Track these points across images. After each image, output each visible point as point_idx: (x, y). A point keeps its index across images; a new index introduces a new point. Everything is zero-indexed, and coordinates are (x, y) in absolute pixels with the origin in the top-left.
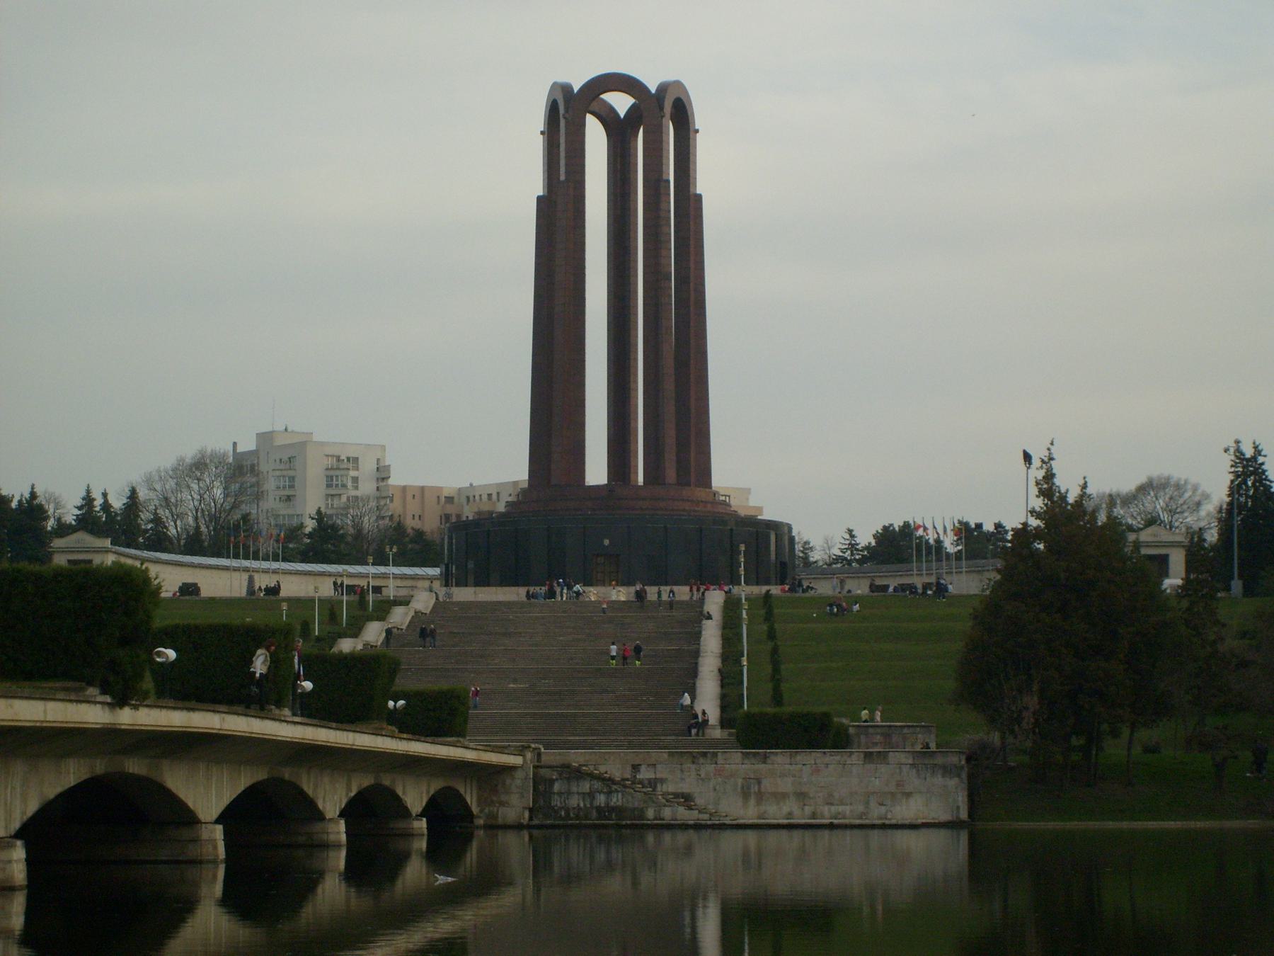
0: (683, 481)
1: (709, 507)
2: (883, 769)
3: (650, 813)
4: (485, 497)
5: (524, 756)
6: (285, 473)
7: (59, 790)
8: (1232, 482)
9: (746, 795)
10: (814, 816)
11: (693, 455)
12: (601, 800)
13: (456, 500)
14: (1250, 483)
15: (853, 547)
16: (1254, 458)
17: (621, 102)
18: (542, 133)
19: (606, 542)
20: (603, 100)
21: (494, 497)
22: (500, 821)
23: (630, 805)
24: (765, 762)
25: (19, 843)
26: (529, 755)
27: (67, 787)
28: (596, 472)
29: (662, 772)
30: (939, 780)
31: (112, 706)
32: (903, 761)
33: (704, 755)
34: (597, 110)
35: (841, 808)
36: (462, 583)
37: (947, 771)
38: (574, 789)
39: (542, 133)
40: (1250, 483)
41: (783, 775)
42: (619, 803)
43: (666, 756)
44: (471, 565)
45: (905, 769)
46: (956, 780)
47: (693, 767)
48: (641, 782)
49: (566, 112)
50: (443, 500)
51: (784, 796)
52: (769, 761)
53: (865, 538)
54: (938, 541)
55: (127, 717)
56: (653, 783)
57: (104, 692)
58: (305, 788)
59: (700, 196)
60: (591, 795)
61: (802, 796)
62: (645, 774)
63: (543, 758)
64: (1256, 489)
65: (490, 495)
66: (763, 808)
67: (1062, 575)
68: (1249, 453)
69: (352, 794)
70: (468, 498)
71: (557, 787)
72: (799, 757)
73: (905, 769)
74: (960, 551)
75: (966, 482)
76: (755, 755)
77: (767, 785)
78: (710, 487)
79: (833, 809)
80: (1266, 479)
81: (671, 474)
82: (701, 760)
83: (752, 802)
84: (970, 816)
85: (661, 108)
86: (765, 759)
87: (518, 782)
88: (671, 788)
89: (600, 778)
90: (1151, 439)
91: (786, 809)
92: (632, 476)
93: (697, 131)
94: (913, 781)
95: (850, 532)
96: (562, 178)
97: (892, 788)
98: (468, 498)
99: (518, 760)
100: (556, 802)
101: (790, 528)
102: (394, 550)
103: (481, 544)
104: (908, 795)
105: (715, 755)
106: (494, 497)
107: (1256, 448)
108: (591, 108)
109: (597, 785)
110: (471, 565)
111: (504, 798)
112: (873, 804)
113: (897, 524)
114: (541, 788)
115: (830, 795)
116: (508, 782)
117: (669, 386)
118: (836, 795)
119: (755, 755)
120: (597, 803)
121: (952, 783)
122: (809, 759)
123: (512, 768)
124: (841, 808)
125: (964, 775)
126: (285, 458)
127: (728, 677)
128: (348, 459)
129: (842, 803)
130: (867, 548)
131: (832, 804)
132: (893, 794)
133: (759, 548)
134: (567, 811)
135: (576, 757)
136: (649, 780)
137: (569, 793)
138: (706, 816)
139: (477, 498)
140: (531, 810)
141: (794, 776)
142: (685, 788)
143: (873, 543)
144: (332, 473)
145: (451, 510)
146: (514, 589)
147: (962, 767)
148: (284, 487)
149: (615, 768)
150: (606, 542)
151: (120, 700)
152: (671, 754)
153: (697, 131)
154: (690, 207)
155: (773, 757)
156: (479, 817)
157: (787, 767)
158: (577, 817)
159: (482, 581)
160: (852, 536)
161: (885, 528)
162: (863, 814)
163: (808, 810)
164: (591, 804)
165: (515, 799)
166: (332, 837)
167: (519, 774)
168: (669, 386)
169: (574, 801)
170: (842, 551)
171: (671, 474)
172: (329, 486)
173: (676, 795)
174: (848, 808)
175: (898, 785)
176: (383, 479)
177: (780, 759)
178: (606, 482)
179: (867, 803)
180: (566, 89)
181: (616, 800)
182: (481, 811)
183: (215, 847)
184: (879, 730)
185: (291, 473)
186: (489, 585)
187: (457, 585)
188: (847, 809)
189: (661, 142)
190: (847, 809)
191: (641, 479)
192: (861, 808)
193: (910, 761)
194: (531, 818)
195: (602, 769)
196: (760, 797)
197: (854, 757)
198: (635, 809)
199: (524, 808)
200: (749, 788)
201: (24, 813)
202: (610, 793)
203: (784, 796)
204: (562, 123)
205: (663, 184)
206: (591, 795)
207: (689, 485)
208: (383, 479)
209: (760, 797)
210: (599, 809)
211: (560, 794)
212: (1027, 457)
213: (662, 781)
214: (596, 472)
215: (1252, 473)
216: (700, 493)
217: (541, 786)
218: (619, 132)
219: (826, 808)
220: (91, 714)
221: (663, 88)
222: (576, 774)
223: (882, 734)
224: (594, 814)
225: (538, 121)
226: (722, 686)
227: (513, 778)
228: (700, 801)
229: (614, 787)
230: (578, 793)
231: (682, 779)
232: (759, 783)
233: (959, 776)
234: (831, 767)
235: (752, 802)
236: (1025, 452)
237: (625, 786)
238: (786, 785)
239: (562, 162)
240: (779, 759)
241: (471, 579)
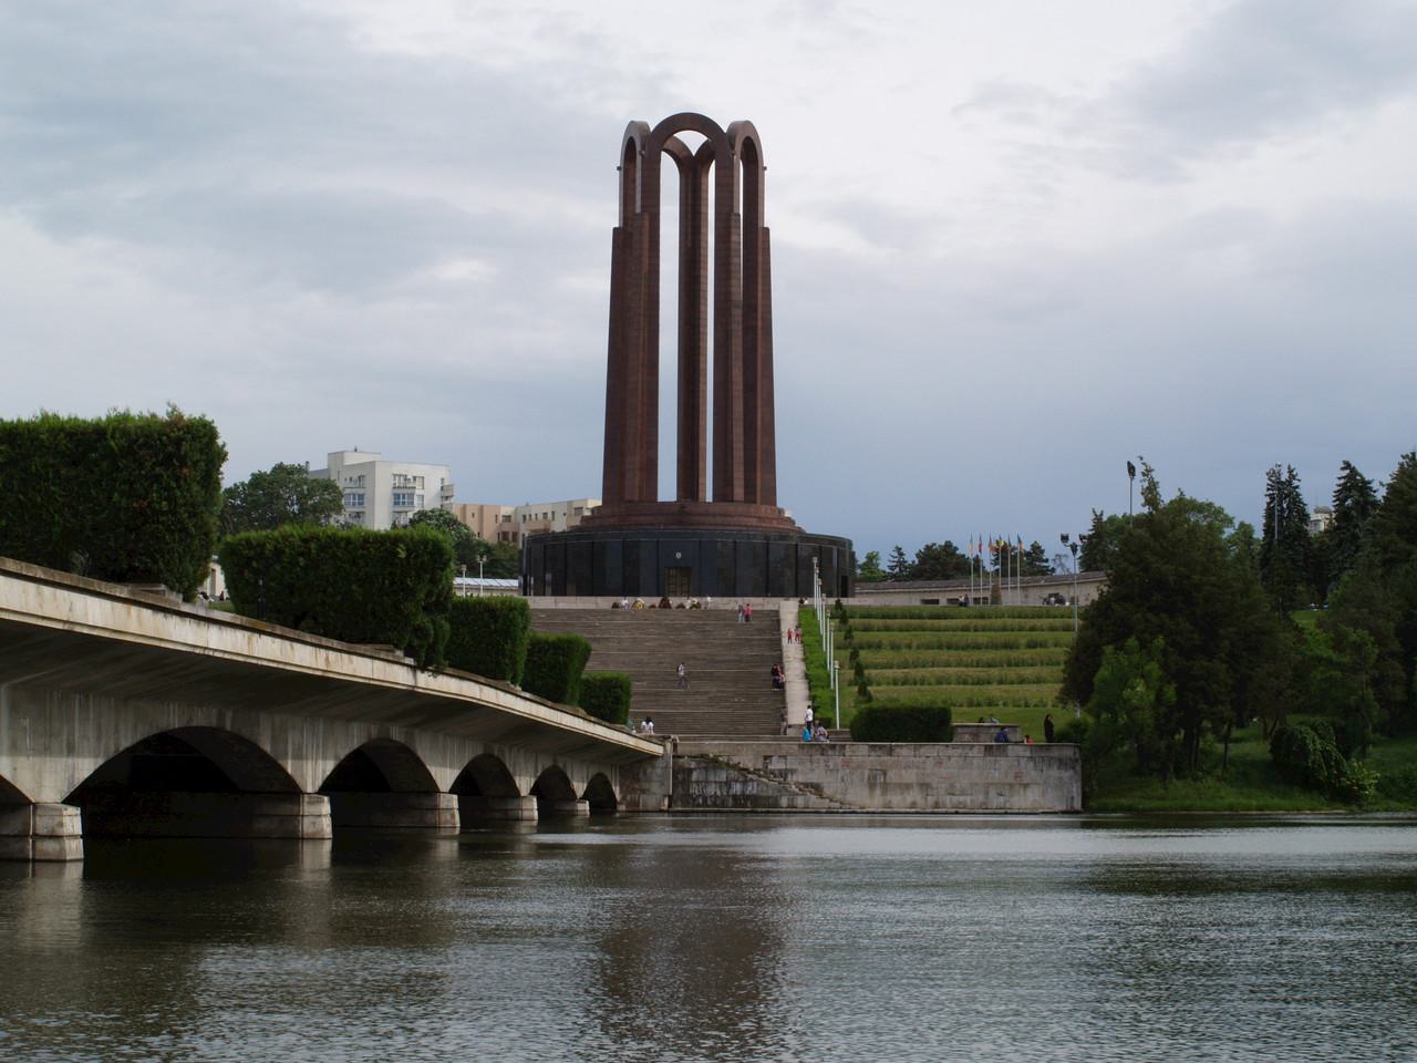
0: (750, 495)
1: (775, 524)
2: (1003, 762)
3: (784, 801)
4: (540, 517)
5: (664, 746)
6: (354, 491)
7: (347, 752)
8: (1269, 504)
9: (872, 786)
10: (936, 805)
11: (759, 474)
12: (737, 788)
13: (513, 518)
14: (1285, 506)
15: (901, 564)
16: (1289, 482)
17: (693, 140)
18: (619, 168)
19: (679, 555)
20: (677, 139)
21: (550, 516)
22: (641, 807)
23: (765, 794)
24: (891, 755)
25: (326, 799)
26: (669, 746)
27: (352, 750)
28: (667, 488)
29: (791, 763)
30: (1055, 772)
31: (414, 668)
32: (1021, 754)
33: (833, 747)
34: (670, 148)
35: (961, 799)
36: (540, 592)
37: (1062, 763)
38: (712, 778)
39: (619, 168)
40: (1285, 506)
41: (907, 767)
42: (755, 792)
43: (796, 748)
44: (549, 577)
45: (1023, 761)
46: (1071, 772)
47: (822, 758)
48: (772, 772)
49: (642, 152)
50: (500, 519)
51: (908, 786)
52: (894, 753)
53: (911, 558)
54: (977, 560)
55: (429, 683)
56: (784, 774)
57: (407, 655)
58: (508, 766)
59: (768, 229)
60: (728, 784)
61: (925, 787)
62: (776, 765)
63: (679, 748)
64: (1290, 512)
65: (545, 514)
66: (888, 798)
67: (1171, 578)
68: (1285, 477)
69: (539, 774)
70: (524, 517)
71: (695, 776)
72: (923, 750)
73: (1023, 761)
74: (997, 570)
75: (1048, 502)
76: (881, 747)
77: (892, 776)
78: (775, 504)
79: (955, 799)
80: (1300, 502)
81: (739, 492)
82: (830, 752)
83: (878, 792)
84: (1083, 805)
85: (733, 147)
86: (890, 752)
87: (659, 771)
88: (801, 779)
89: (735, 767)
90: (1339, 442)
91: (909, 799)
92: (700, 494)
93: (765, 168)
94: (1030, 772)
95: (899, 549)
96: (638, 210)
97: (1011, 779)
98: (524, 517)
99: (657, 749)
100: (694, 790)
101: (850, 543)
102: (485, 559)
103: (561, 557)
104: (1026, 786)
105: (844, 746)
106: (550, 516)
107: (1290, 471)
108: (665, 146)
109: (734, 774)
110: (549, 577)
111: (645, 786)
112: (992, 793)
113: (922, 548)
114: (680, 777)
115: (952, 786)
116: (649, 771)
117: (738, 408)
118: (958, 785)
119: (881, 747)
120: (732, 792)
121: (1067, 774)
122: (931, 751)
123: (653, 757)
124: (961, 799)
125: (1078, 768)
126: (355, 477)
127: (816, 681)
128: (415, 478)
129: (963, 793)
130: (910, 567)
131: (953, 795)
132: (1011, 785)
133: (825, 564)
134: (705, 800)
135: (712, 747)
136: (780, 770)
137: (707, 782)
138: (838, 805)
139: (533, 517)
140: (670, 797)
141: (918, 768)
142: (813, 778)
143: (917, 562)
144: (400, 491)
145: (507, 528)
146: (593, 598)
147: (1077, 760)
148: (354, 504)
149: (747, 760)
150: (679, 555)
151: (421, 667)
152: (802, 747)
153: (765, 168)
154: (757, 238)
155: (897, 750)
156: (621, 804)
157: (913, 758)
158: (715, 805)
159: (559, 591)
160: (901, 554)
161: (928, 548)
162: (985, 804)
163: (931, 800)
164: (728, 792)
165: (655, 787)
166: (526, 814)
167: (660, 763)
168: (738, 408)
169: (712, 790)
170: (891, 568)
171: (739, 492)
172: (396, 503)
173: (807, 785)
174: (968, 799)
175: (1016, 777)
176: (447, 498)
177: (905, 751)
178: (675, 499)
179: (987, 793)
180: (642, 127)
181: (752, 789)
182: (624, 798)
183: (453, 816)
184: (965, 730)
185: (361, 491)
186: (565, 594)
187: (535, 595)
188: (968, 799)
189: (732, 176)
190: (968, 799)
191: (709, 498)
192: (981, 798)
193: (1028, 754)
194: (670, 806)
195: (735, 760)
196: (885, 787)
197: (975, 750)
198: (769, 797)
199: (665, 796)
200: (875, 778)
201: (324, 771)
202: (745, 782)
203: (908, 786)
204: (639, 158)
205: (733, 217)
206: (728, 784)
207: (755, 502)
208: (447, 498)
209: (885, 787)
210: (735, 797)
211: (697, 782)
212: (1131, 470)
213: (793, 771)
214: (667, 488)
215: (1287, 496)
216: (764, 510)
217: (681, 775)
218: (691, 168)
219: (948, 797)
220: (396, 674)
221: (734, 127)
222: (713, 763)
223: (971, 734)
224: (731, 801)
225: (616, 157)
226: (810, 689)
227: (654, 767)
228: (827, 791)
229: (750, 776)
230: (716, 782)
231: (812, 770)
232: (885, 774)
233: (1073, 768)
234: (953, 759)
235: (878, 792)
236: (1129, 463)
237: (760, 776)
238: (910, 776)
239: (638, 196)
240: (904, 752)
241: (549, 590)
